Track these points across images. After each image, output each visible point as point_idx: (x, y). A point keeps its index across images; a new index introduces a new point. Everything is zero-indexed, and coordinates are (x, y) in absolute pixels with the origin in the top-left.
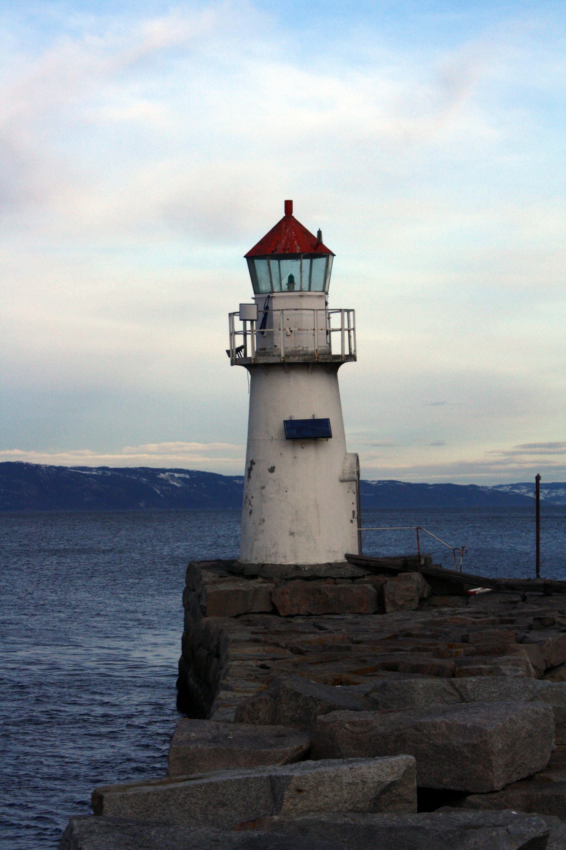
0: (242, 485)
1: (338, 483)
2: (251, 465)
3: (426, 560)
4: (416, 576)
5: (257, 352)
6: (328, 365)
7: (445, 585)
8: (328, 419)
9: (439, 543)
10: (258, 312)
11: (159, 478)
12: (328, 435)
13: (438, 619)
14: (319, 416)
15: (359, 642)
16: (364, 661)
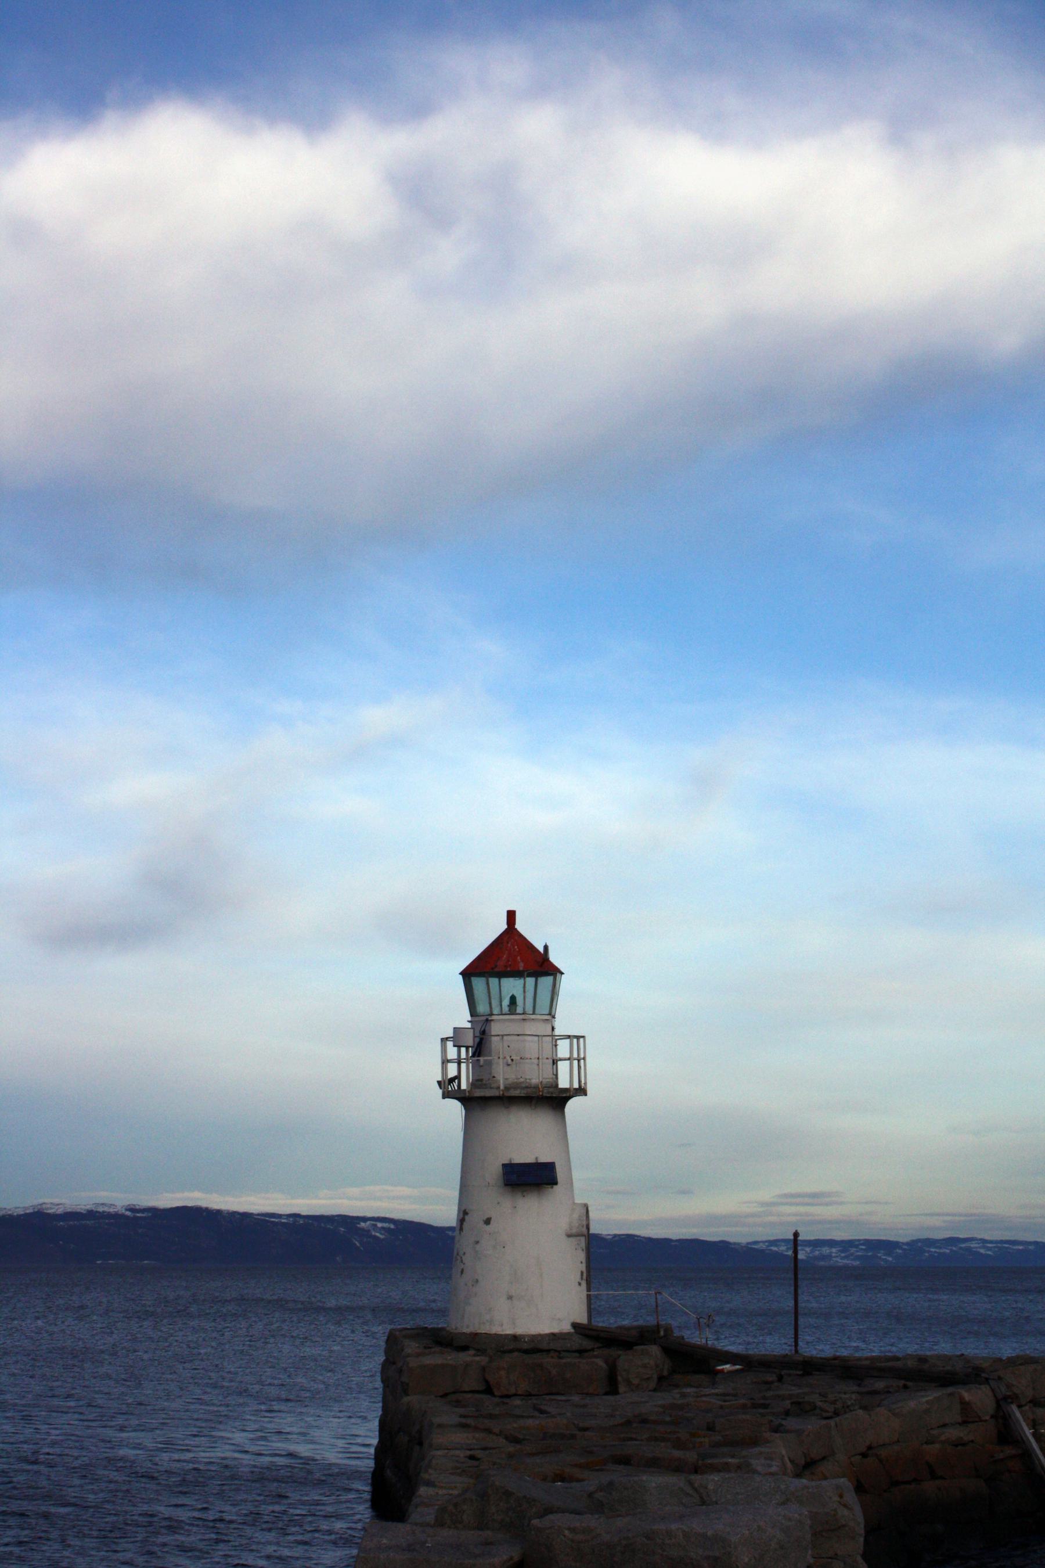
0: (453, 1238)
1: (564, 1237)
2: (463, 1215)
3: (666, 1331)
4: (655, 1350)
5: (472, 1084)
6: (554, 1100)
7: (690, 1362)
9: (686, 1313)
10: (475, 1037)
11: (360, 1229)
12: (553, 1182)
13: (680, 1402)
14: (543, 1159)
15: (586, 1429)
16: (591, 1452)
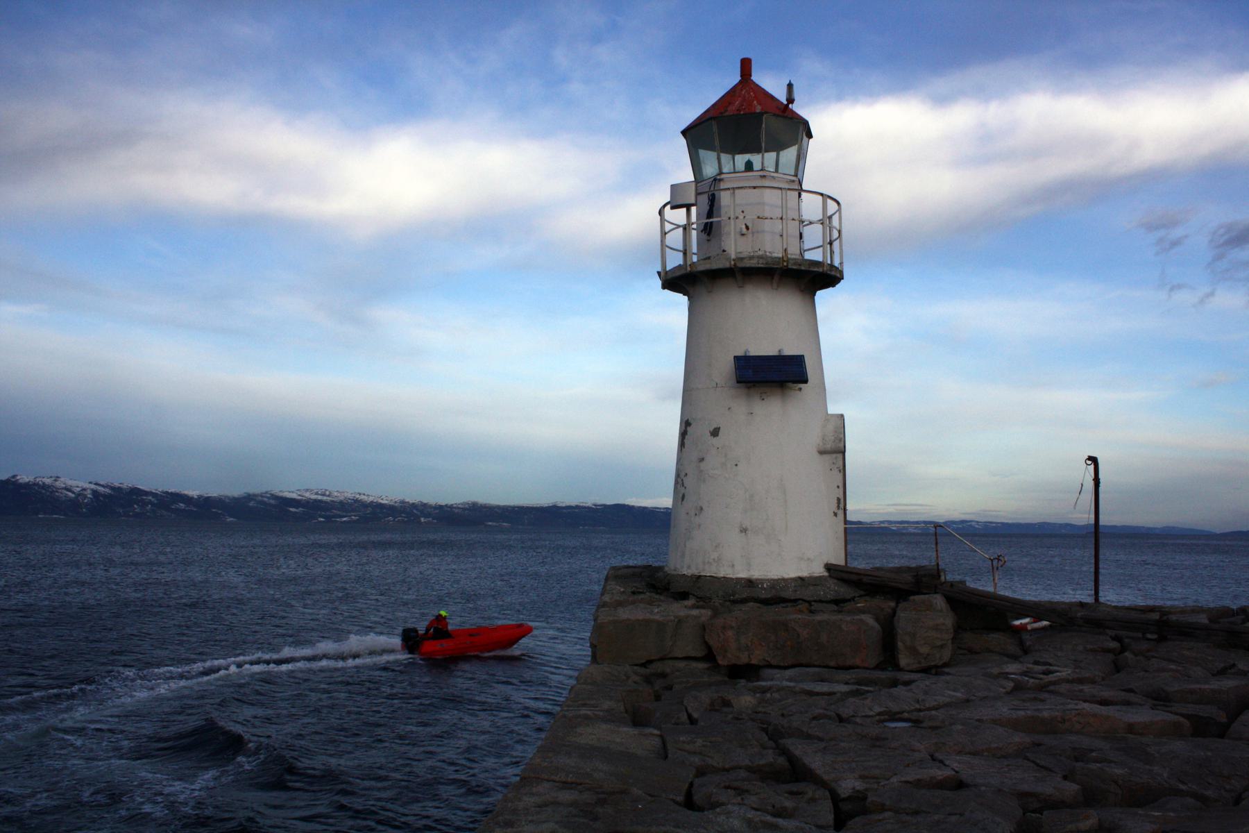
8: (802, 357)
14: (788, 351)
